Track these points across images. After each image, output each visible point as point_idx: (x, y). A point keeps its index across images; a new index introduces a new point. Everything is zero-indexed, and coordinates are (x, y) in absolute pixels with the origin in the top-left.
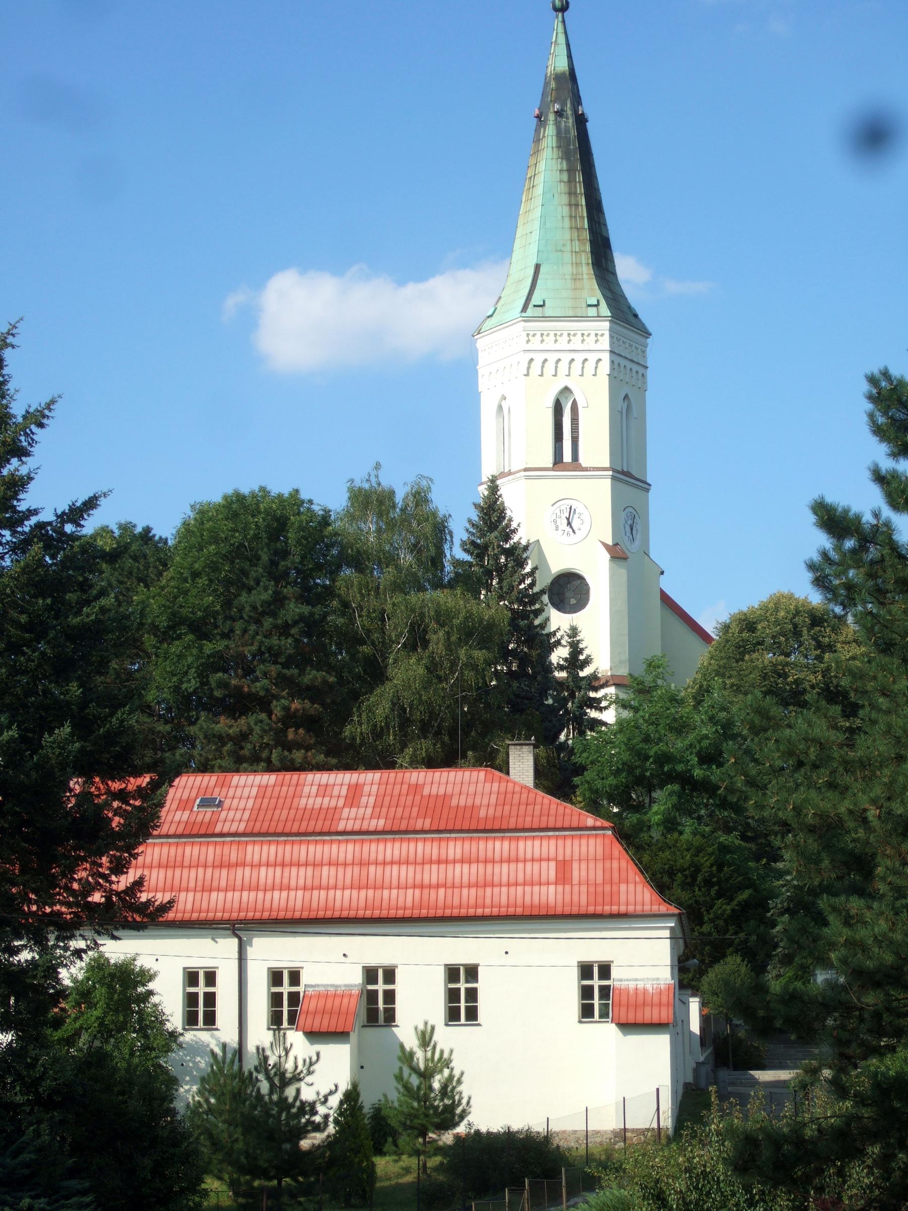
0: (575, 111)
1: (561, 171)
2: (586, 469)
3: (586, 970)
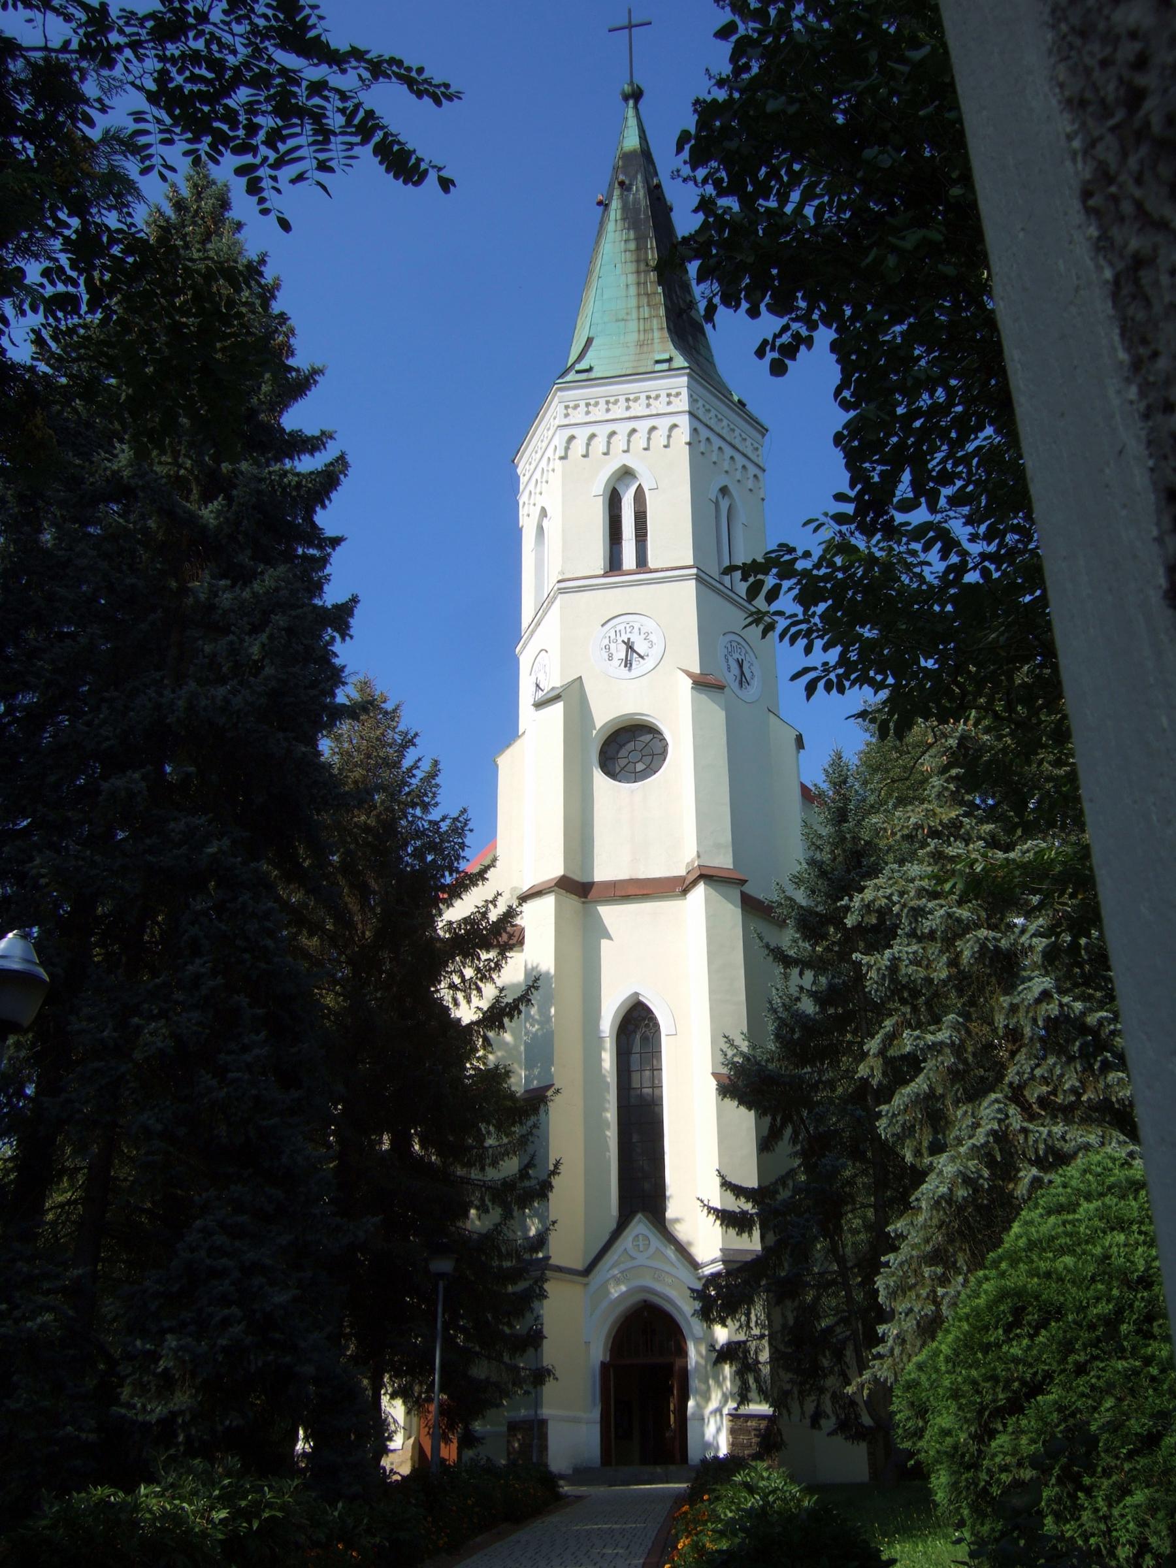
0: (647, 181)
1: (626, 241)
2: (656, 571)
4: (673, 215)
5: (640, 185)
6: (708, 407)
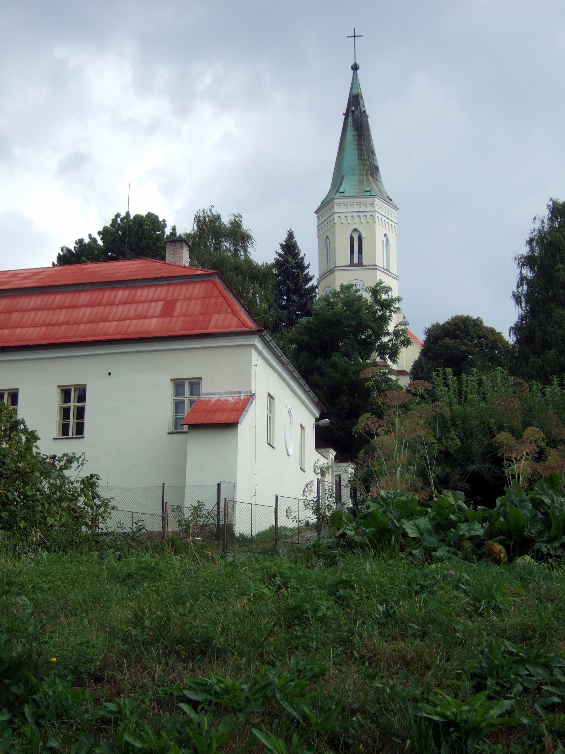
2: (365, 266)
3: (178, 385)
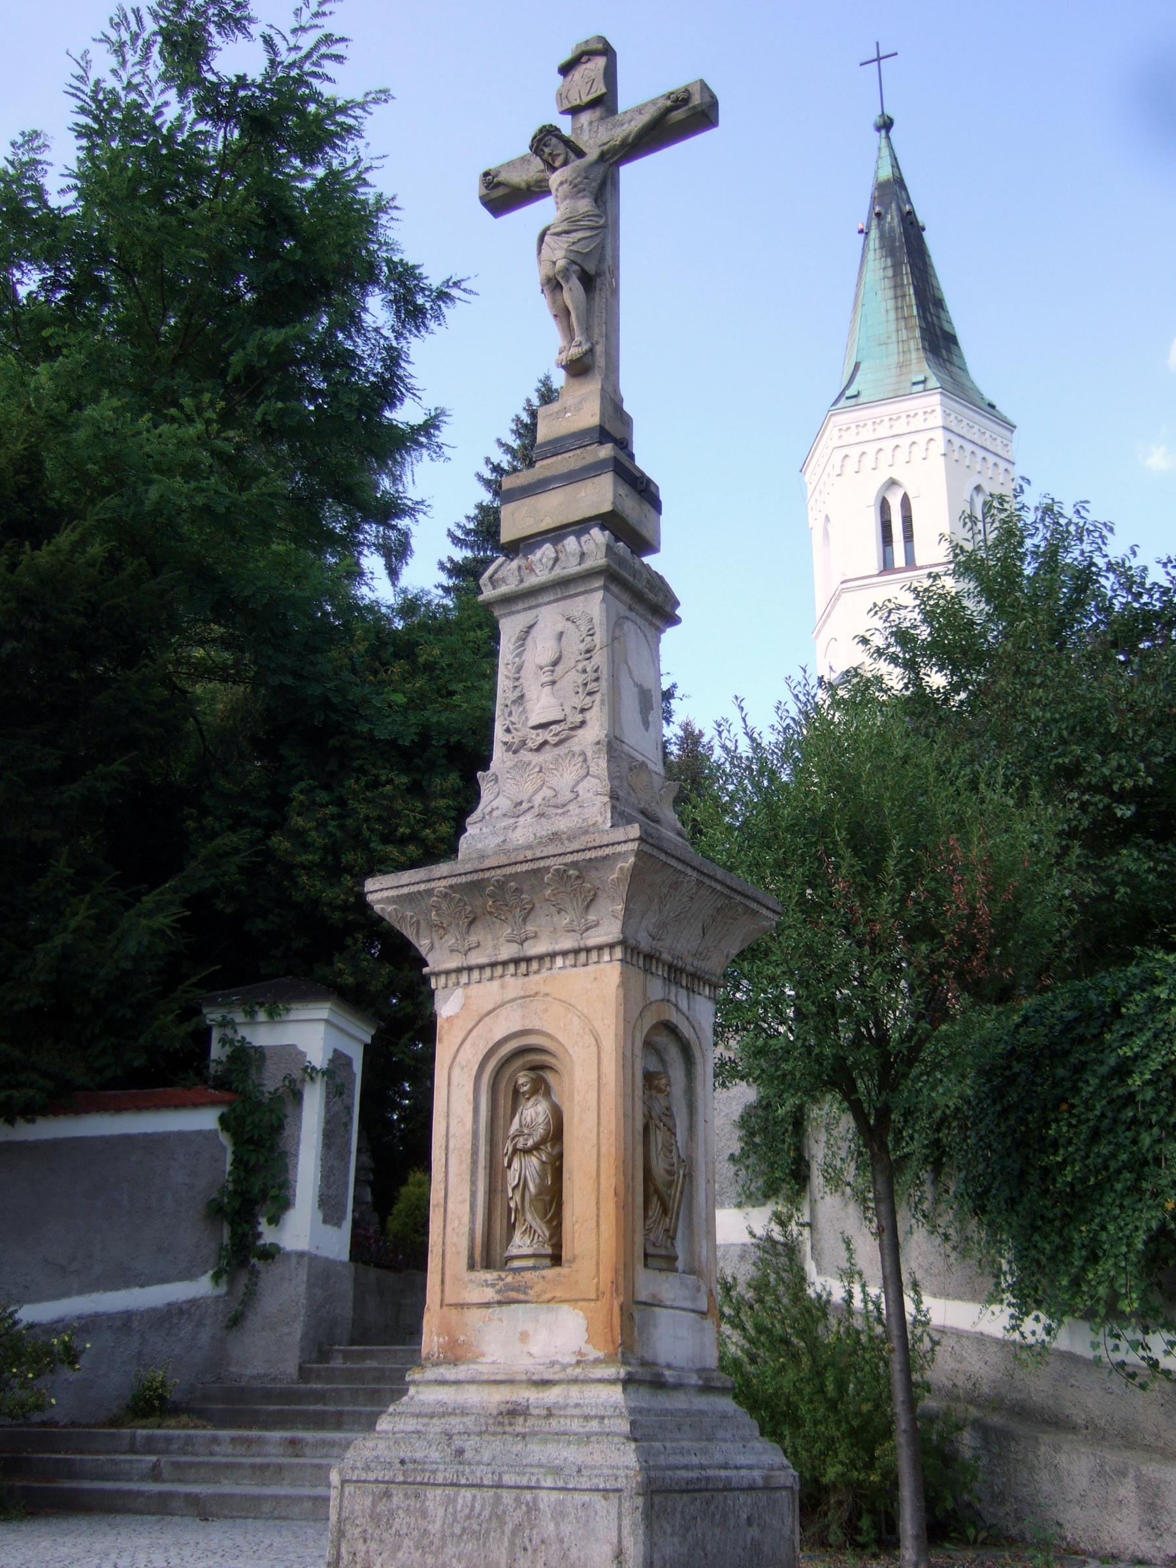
4: (924, 234)
5: (895, 213)
6: (960, 418)
